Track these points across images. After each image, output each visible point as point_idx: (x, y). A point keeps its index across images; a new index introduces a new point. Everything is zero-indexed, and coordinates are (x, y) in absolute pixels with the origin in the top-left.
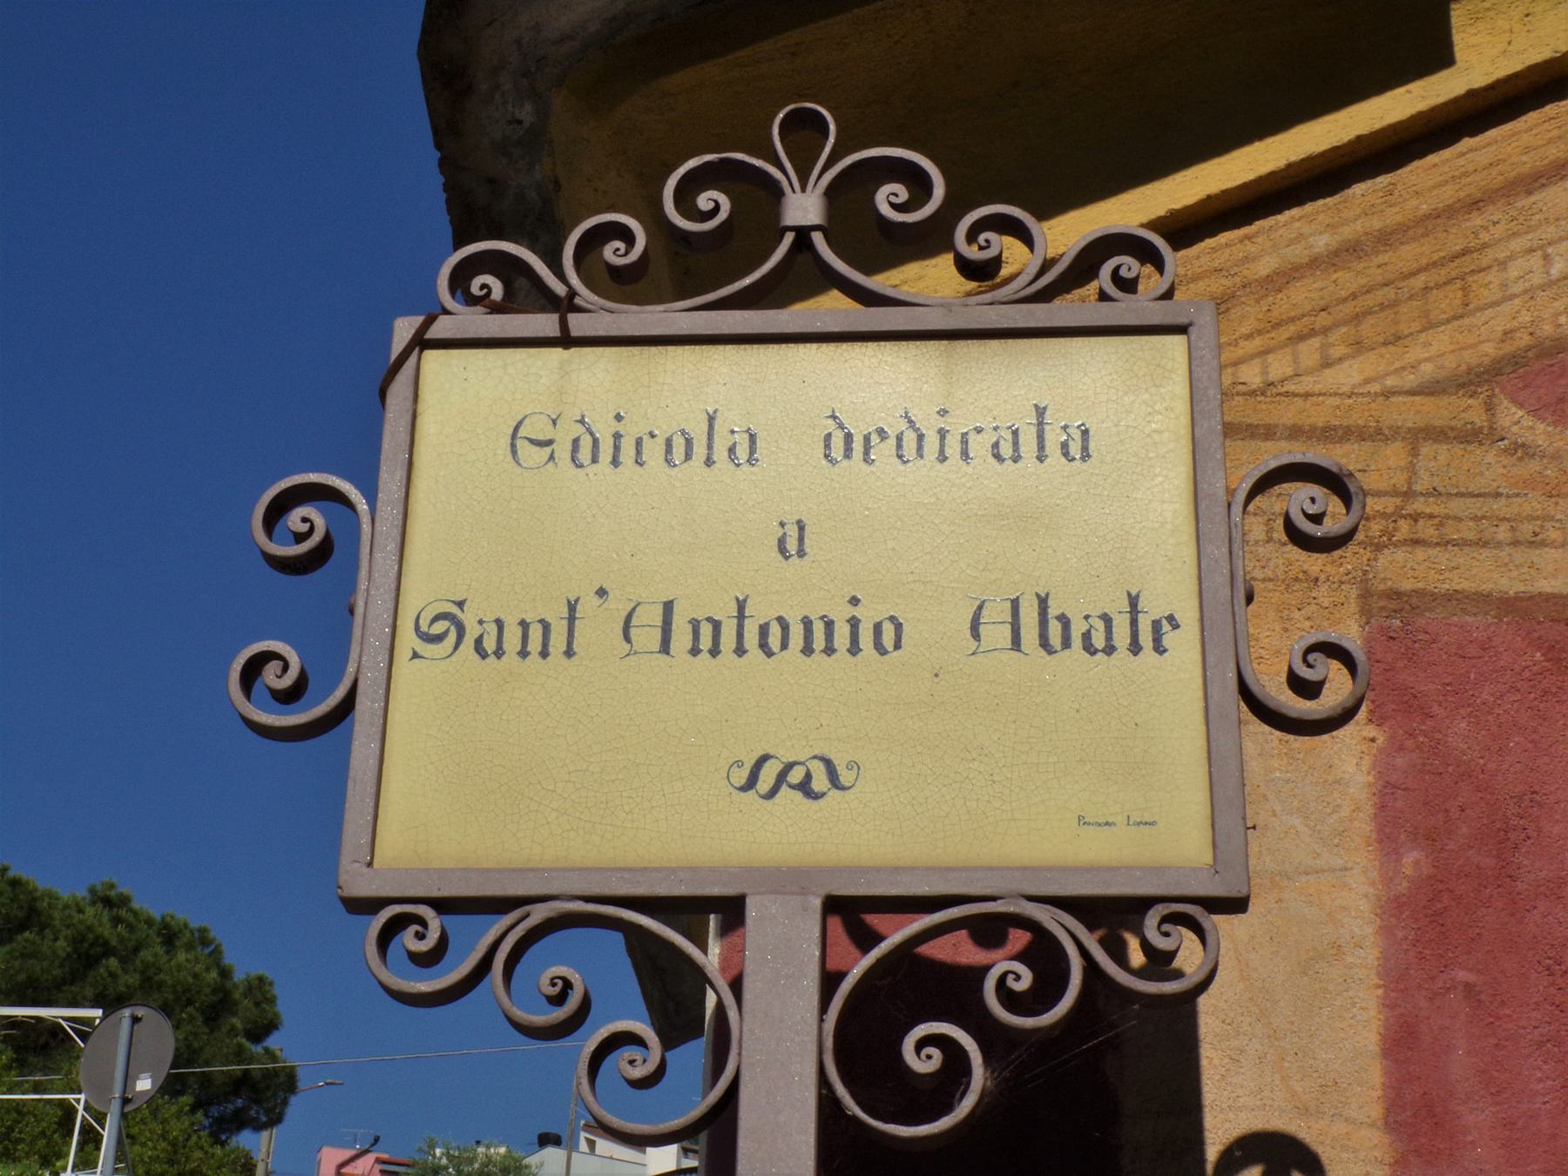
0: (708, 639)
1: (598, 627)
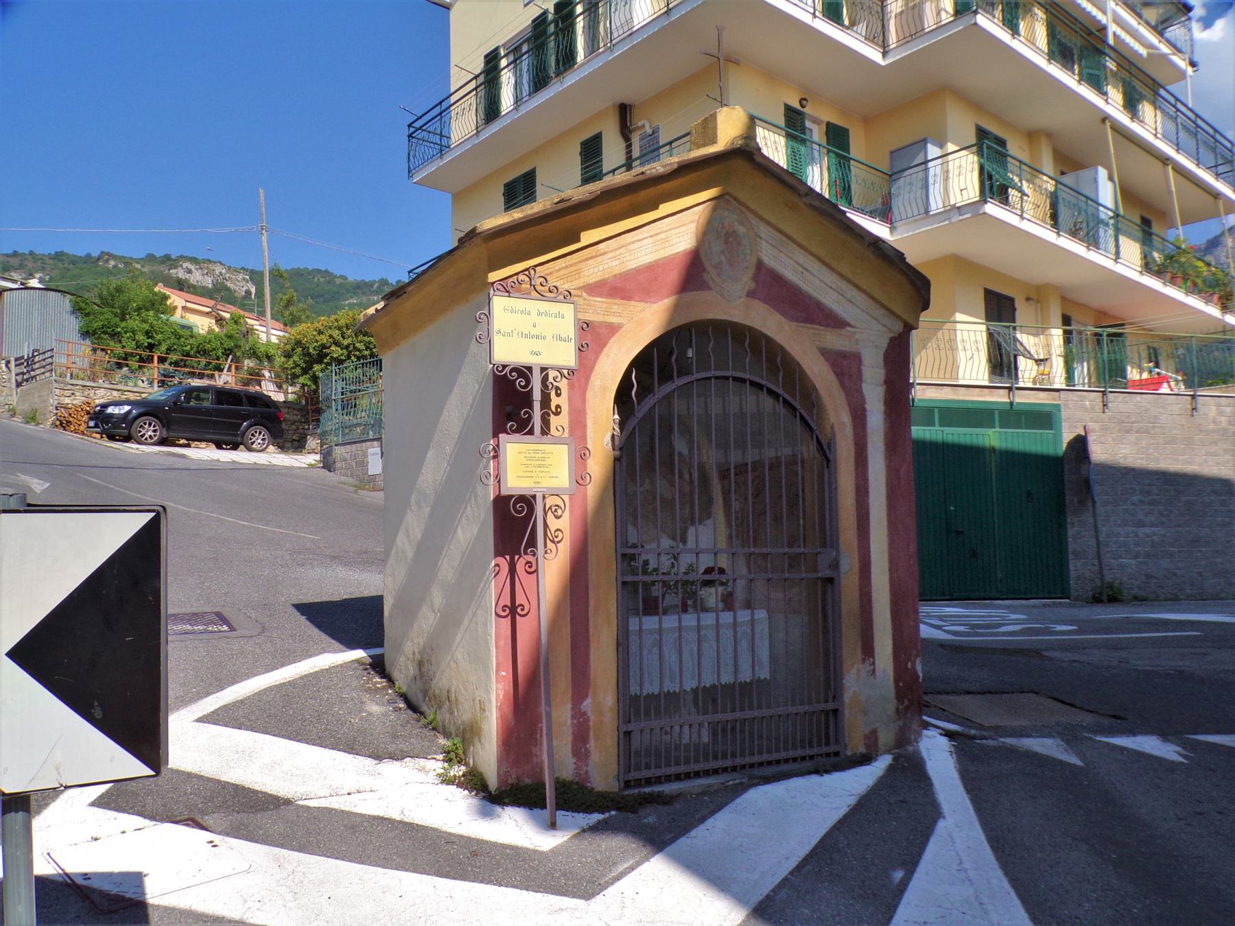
1: (515, 333)
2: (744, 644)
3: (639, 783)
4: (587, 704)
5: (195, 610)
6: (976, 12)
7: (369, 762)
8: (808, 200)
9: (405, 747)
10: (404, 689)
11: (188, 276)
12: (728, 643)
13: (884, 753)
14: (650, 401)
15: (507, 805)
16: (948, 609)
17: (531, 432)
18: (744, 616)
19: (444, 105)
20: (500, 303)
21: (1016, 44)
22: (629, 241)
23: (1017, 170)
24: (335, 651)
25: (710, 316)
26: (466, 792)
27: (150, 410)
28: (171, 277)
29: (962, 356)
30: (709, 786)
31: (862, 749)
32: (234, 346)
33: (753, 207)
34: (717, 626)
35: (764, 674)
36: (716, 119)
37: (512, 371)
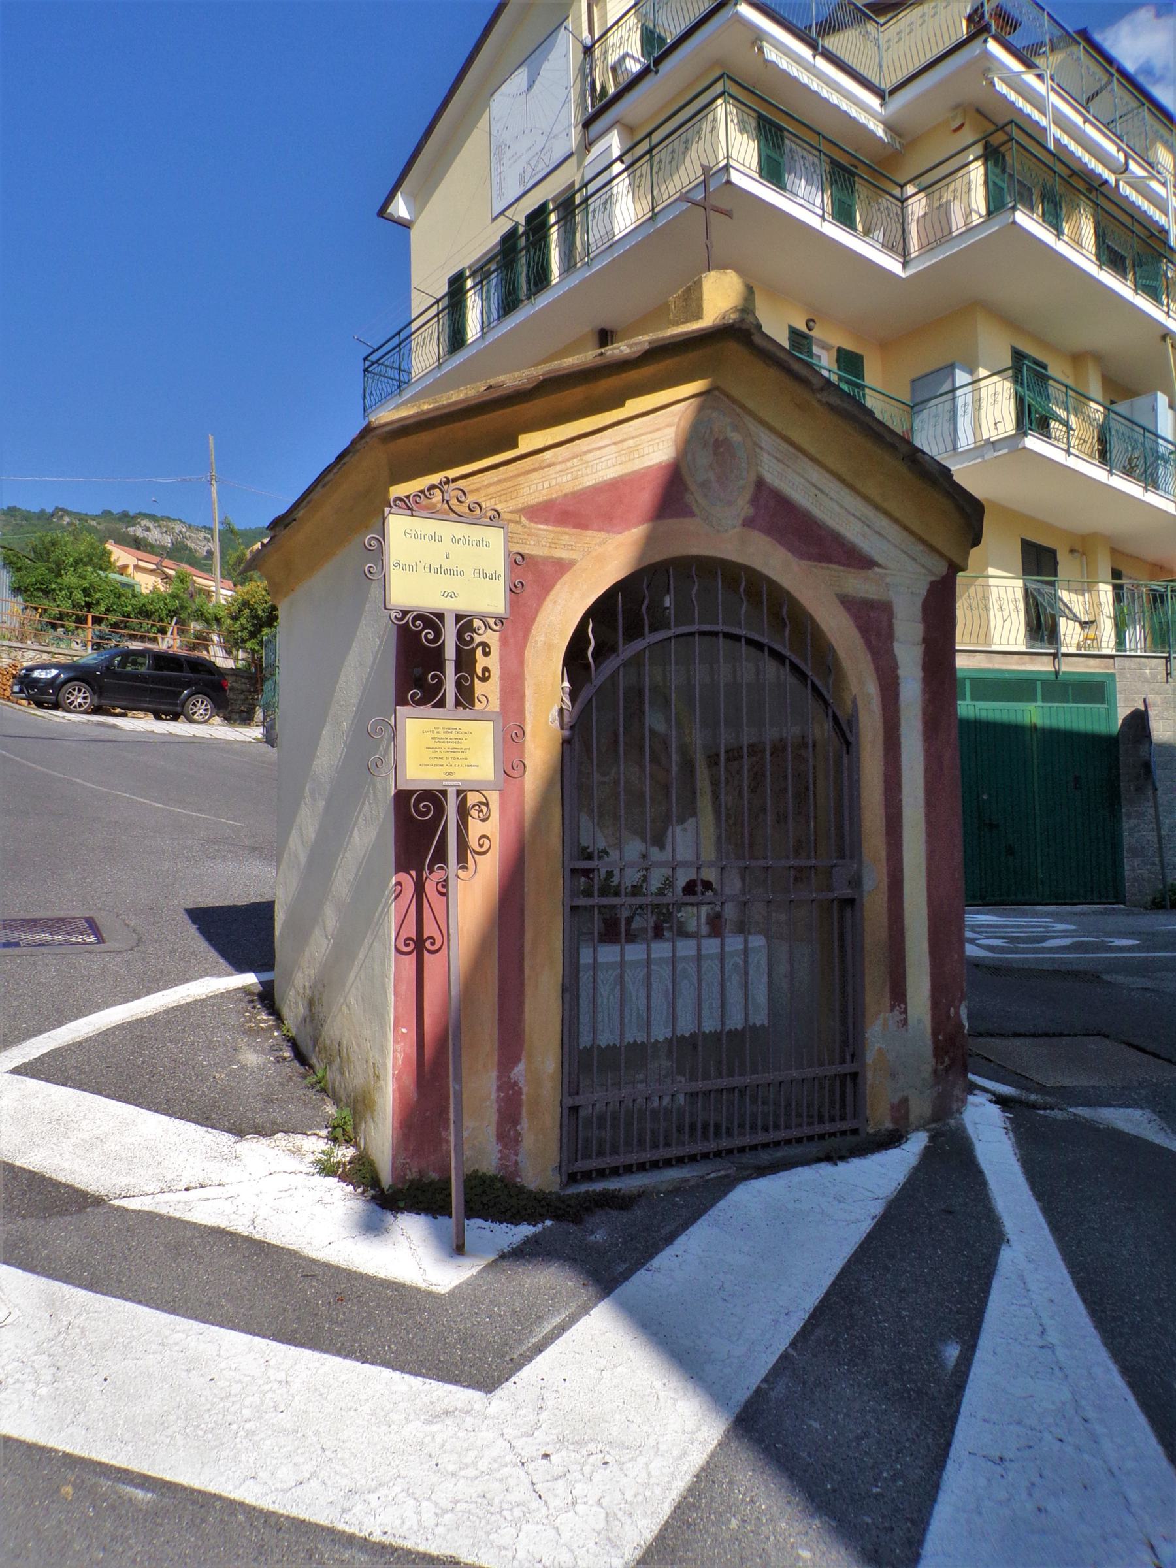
0: (436, 571)
1: (420, 567)
2: (734, 981)
3: (587, 1176)
4: (519, 1072)
5: (62, 914)
6: (1014, 208)
7: (226, 1138)
8: (824, 397)
9: (277, 1116)
10: (293, 1032)
11: (146, 534)
12: (712, 981)
13: (917, 1129)
14: (612, 664)
15: (400, 1210)
16: (980, 917)
17: (441, 704)
18: (734, 943)
19: (404, 335)
20: (398, 525)
21: (1062, 248)
22: (585, 448)
23: (1062, 397)
24: (220, 975)
25: (694, 551)
26: (351, 1188)
27: (81, 675)
28: (129, 535)
29: (995, 617)
30: (685, 1180)
31: (888, 1125)
32: (178, 609)
33: (750, 405)
34: (699, 957)
35: (760, 1018)
36: (701, 287)
37: (416, 618)
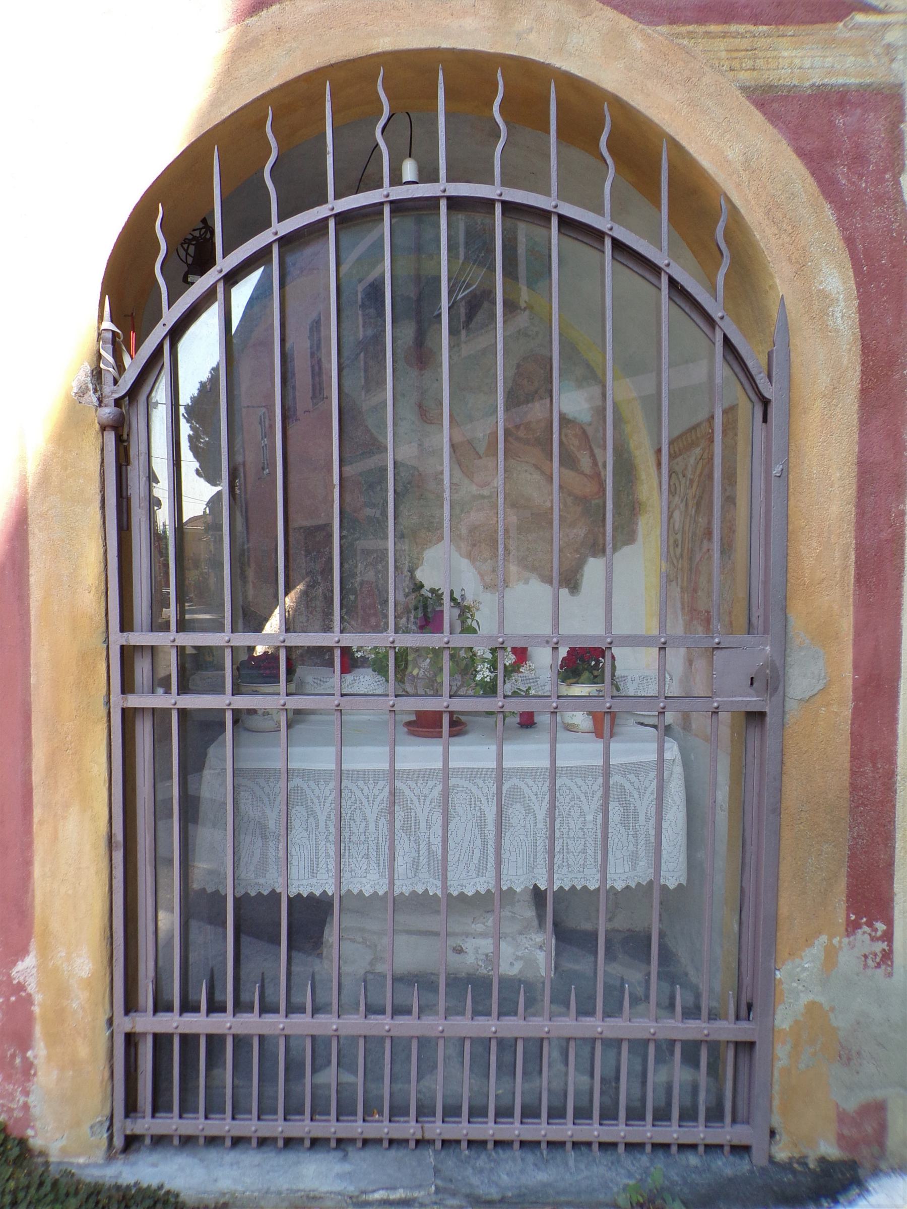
31: (830, 1150)
